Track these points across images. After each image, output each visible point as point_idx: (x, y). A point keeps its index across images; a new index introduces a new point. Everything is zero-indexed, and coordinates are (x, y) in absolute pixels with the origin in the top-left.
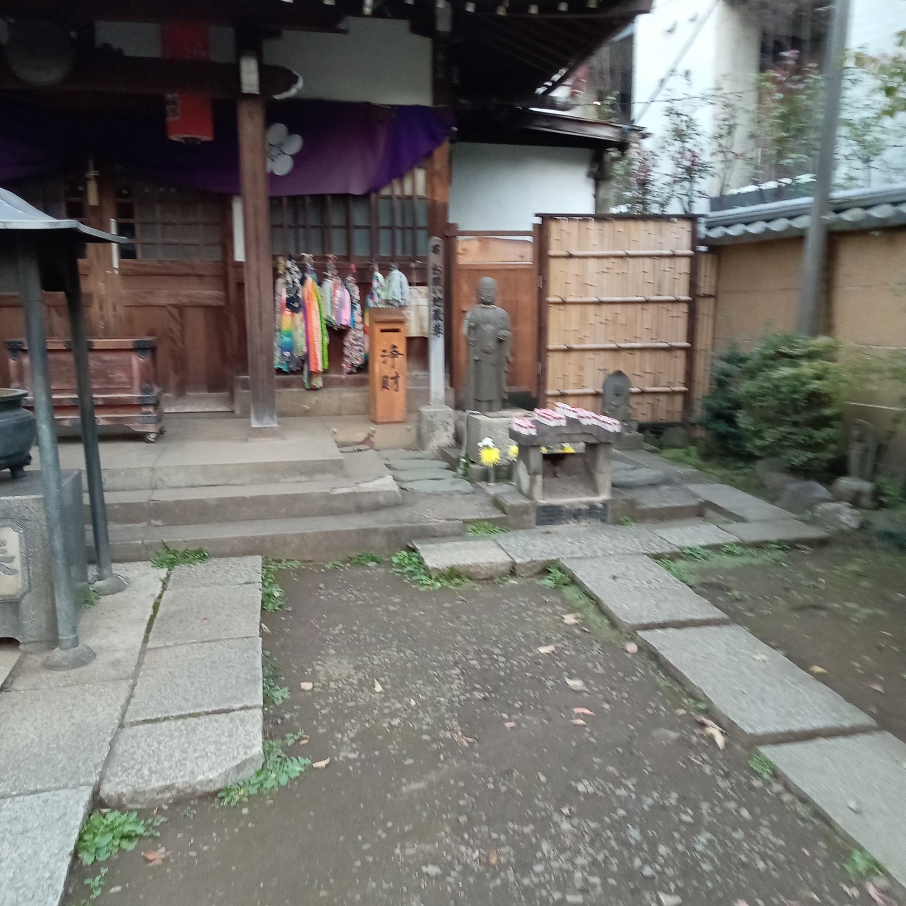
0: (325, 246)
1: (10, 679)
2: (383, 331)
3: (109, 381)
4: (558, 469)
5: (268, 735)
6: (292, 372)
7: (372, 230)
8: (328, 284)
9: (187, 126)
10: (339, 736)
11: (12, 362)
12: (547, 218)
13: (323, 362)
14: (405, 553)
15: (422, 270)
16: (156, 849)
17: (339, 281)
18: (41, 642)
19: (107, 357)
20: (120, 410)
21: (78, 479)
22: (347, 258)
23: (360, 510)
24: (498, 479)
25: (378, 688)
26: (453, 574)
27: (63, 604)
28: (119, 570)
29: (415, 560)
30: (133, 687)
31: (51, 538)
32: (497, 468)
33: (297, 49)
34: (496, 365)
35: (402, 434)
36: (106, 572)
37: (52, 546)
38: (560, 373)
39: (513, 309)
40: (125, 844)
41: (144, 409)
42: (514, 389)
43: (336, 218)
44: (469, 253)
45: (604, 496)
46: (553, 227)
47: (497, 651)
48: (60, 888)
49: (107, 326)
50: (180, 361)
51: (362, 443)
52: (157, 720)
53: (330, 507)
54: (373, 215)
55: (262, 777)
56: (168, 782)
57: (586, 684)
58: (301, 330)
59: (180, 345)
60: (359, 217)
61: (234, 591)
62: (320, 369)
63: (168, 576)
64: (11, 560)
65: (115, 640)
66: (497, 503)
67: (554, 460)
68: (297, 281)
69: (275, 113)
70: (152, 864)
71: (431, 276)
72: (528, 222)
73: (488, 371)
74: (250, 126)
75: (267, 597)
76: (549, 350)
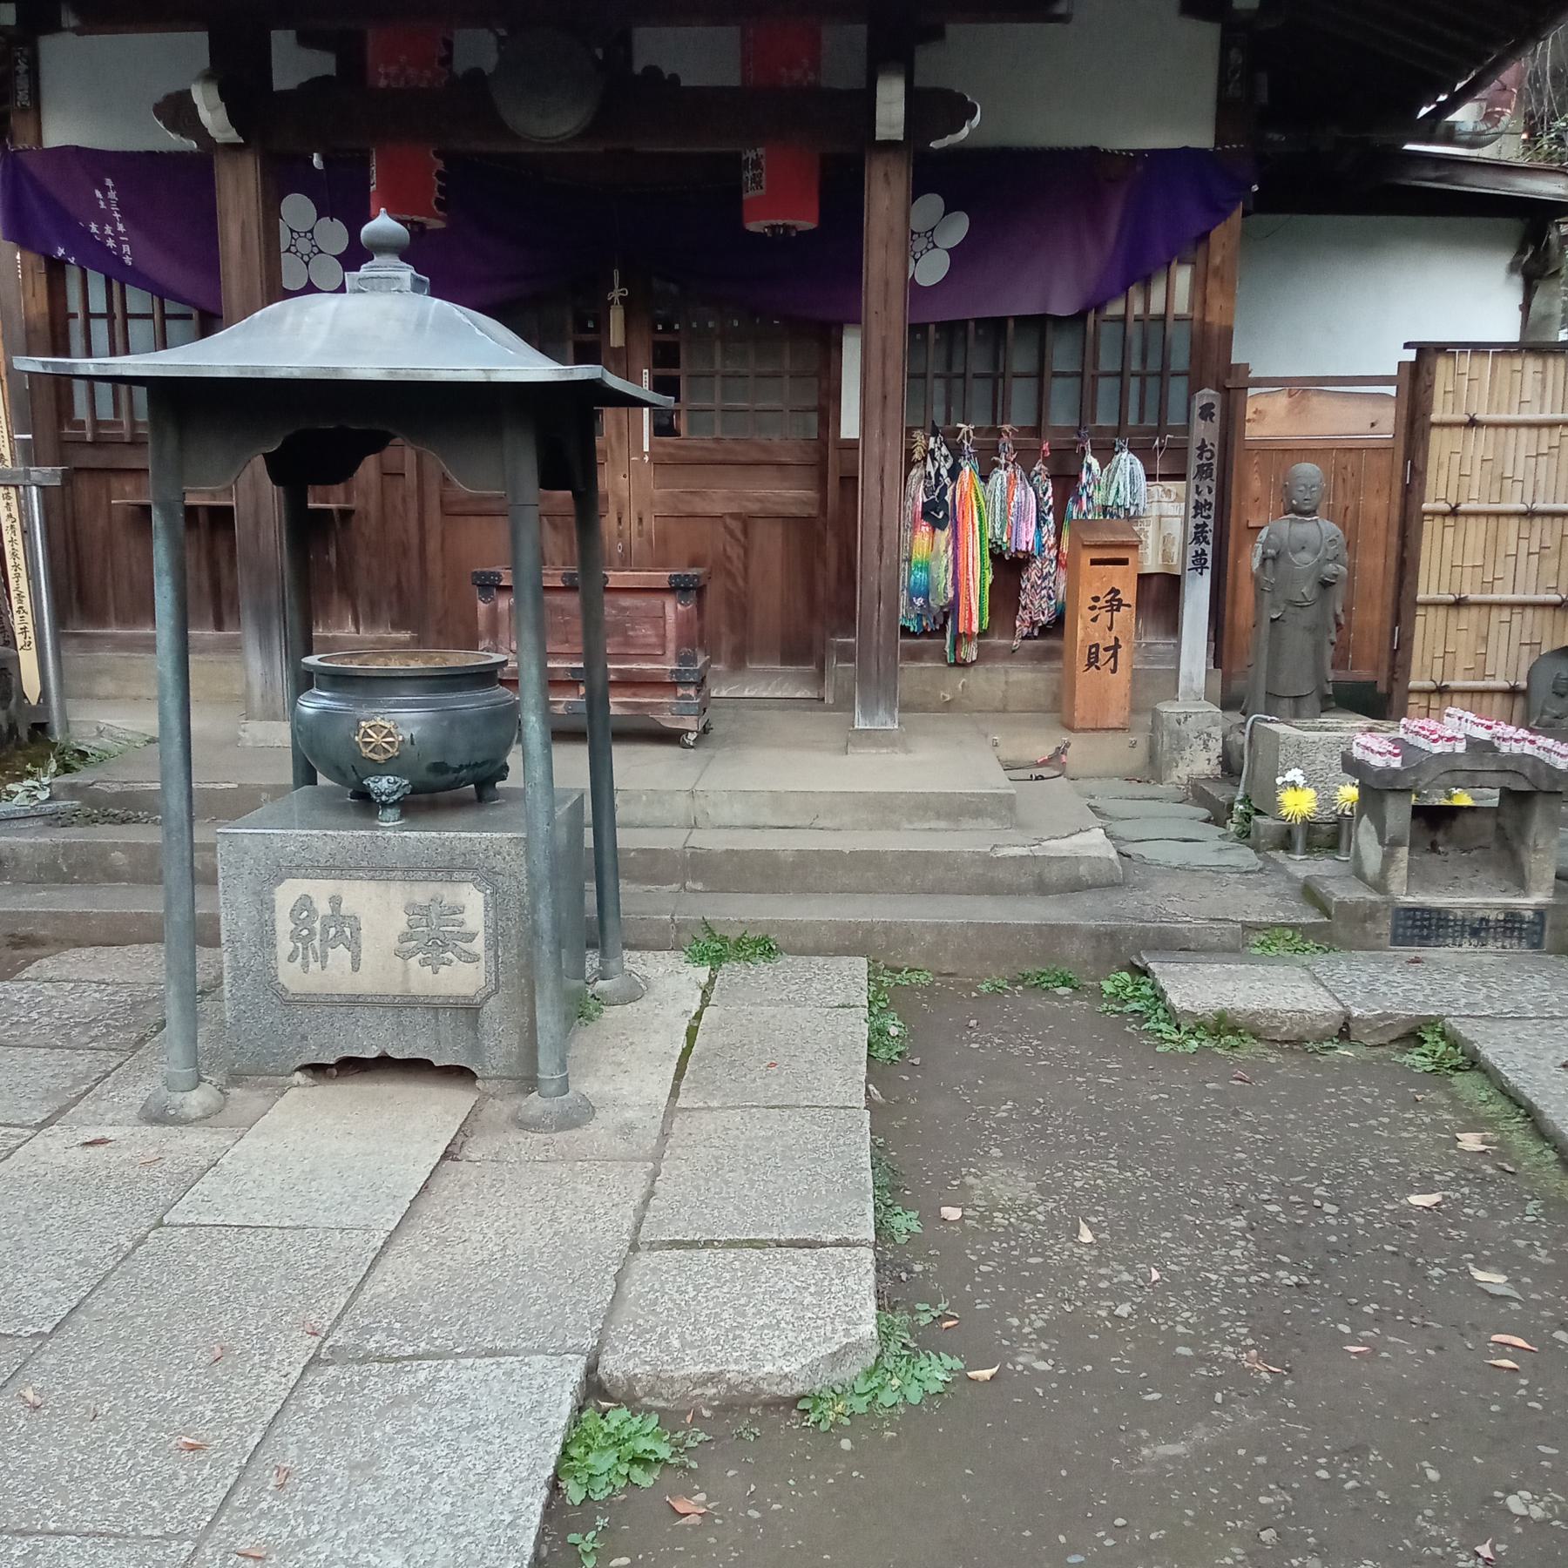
0: (998, 409)
1: (459, 1140)
2: (1093, 562)
3: (628, 642)
4: (1440, 837)
5: (886, 1302)
7: (1087, 379)
8: (1000, 477)
10: (1015, 1322)
11: (482, 606)
12: (1427, 353)
14: (1125, 975)
15: (1178, 452)
16: (690, 1494)
17: (1019, 472)
19: (626, 601)
20: (640, 691)
21: (579, 803)
22: (1037, 431)
23: (1042, 888)
24: (1310, 847)
25: (1086, 1236)
26: (1223, 1026)
27: (547, 1020)
28: (636, 962)
29: (1146, 990)
30: (655, 1174)
31: (534, 909)
32: (1310, 826)
33: (970, 55)
34: (1312, 630)
35: (1119, 752)
36: (613, 965)
37: (534, 921)
38: (1436, 647)
39: (1351, 522)
40: (637, 1473)
41: (681, 691)
42: (1344, 675)
43: (1021, 359)
44: (1268, 418)
45: (1539, 897)
46: (1442, 367)
47: (1320, 1191)
48: (529, 1550)
49: (627, 549)
50: (740, 610)
51: (1044, 764)
52: (693, 1245)
53: (989, 879)
54: (1088, 351)
55: (875, 1382)
56: (713, 1369)
57: (1514, 1281)
58: (946, 559)
59: (741, 582)
60: (1062, 354)
61: (820, 1020)
62: (975, 628)
63: (712, 981)
64: (471, 937)
65: (626, 1087)
66: (1310, 894)
67: (1434, 820)
68: (944, 472)
70: (684, 1520)
71: (1194, 463)
72: (1390, 358)
73: (1297, 641)
74: (885, 197)
76: (1417, 604)
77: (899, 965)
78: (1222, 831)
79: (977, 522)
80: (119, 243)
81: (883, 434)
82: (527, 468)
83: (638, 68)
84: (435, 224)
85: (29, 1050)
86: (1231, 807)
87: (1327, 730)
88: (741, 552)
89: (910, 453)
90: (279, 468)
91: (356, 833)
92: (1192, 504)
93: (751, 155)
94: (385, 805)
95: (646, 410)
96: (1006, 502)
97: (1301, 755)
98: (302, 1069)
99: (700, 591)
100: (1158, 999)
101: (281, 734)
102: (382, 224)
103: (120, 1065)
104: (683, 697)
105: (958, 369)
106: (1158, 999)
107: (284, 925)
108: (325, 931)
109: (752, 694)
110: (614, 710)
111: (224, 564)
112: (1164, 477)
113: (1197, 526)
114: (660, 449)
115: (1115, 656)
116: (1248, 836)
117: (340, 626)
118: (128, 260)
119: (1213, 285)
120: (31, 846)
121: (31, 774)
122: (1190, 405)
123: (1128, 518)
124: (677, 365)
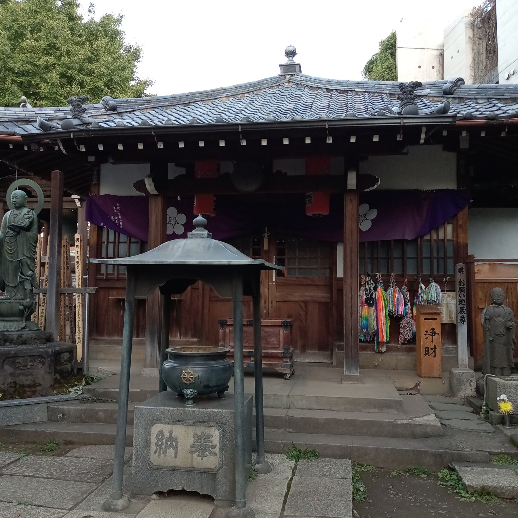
0: (389, 269)
2: (425, 319)
3: (267, 343)
6: (367, 341)
8: (391, 290)
9: (317, 207)
13: (387, 337)
17: (397, 289)
18: (225, 500)
19: (267, 329)
22: (403, 275)
23: (414, 436)
26: (484, 492)
27: (239, 478)
28: (269, 458)
29: (454, 477)
31: (236, 438)
32: (511, 416)
35: (439, 386)
36: (261, 459)
37: (236, 442)
41: (285, 360)
43: (396, 253)
44: (482, 273)
51: (411, 389)
53: (394, 432)
58: (374, 317)
59: (304, 323)
60: (410, 252)
61: (334, 481)
62: (385, 340)
64: (214, 447)
65: (266, 506)
68: (372, 288)
69: (364, 198)
71: (458, 287)
74: (350, 207)
75: (357, 489)
77: (363, 463)
78: (479, 417)
79: (384, 305)
80: (119, 222)
81: (351, 276)
82: (240, 291)
83: (274, 171)
84: (213, 215)
85: (68, 482)
86: (481, 408)
87: (514, 380)
88: (304, 313)
89: (360, 282)
90: (163, 290)
91: (179, 409)
92: (458, 300)
93: (308, 194)
94: (189, 399)
95: (274, 271)
96: (393, 298)
97: (505, 389)
98: (155, 493)
99: (291, 326)
100: (459, 480)
101: (155, 373)
102: (200, 218)
103: (96, 489)
104: (285, 362)
105: (375, 256)
106: (459, 480)
107: (154, 440)
108: (167, 443)
109: (308, 361)
110: (263, 366)
111: (141, 316)
112: (447, 291)
113: (460, 308)
114: (278, 281)
115: (435, 351)
116: (488, 418)
117: (175, 336)
118: (121, 227)
119: (460, 230)
120: (75, 409)
121: (76, 385)
122: (455, 268)
123: (436, 304)
124: (284, 255)
